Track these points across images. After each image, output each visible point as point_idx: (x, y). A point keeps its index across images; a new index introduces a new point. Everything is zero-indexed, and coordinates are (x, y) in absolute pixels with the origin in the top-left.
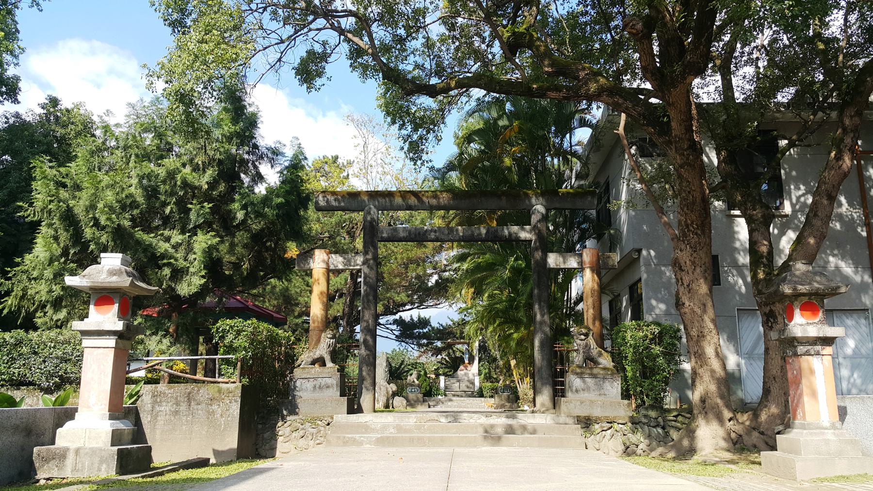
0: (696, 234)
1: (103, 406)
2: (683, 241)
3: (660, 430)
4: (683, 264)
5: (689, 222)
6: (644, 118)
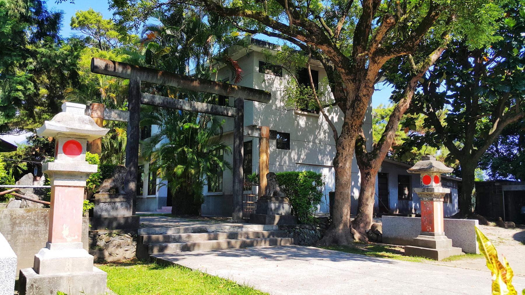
0: (355, 131)
1: (76, 237)
2: (347, 134)
3: (313, 232)
4: (345, 146)
5: (354, 124)
6: (342, 64)
